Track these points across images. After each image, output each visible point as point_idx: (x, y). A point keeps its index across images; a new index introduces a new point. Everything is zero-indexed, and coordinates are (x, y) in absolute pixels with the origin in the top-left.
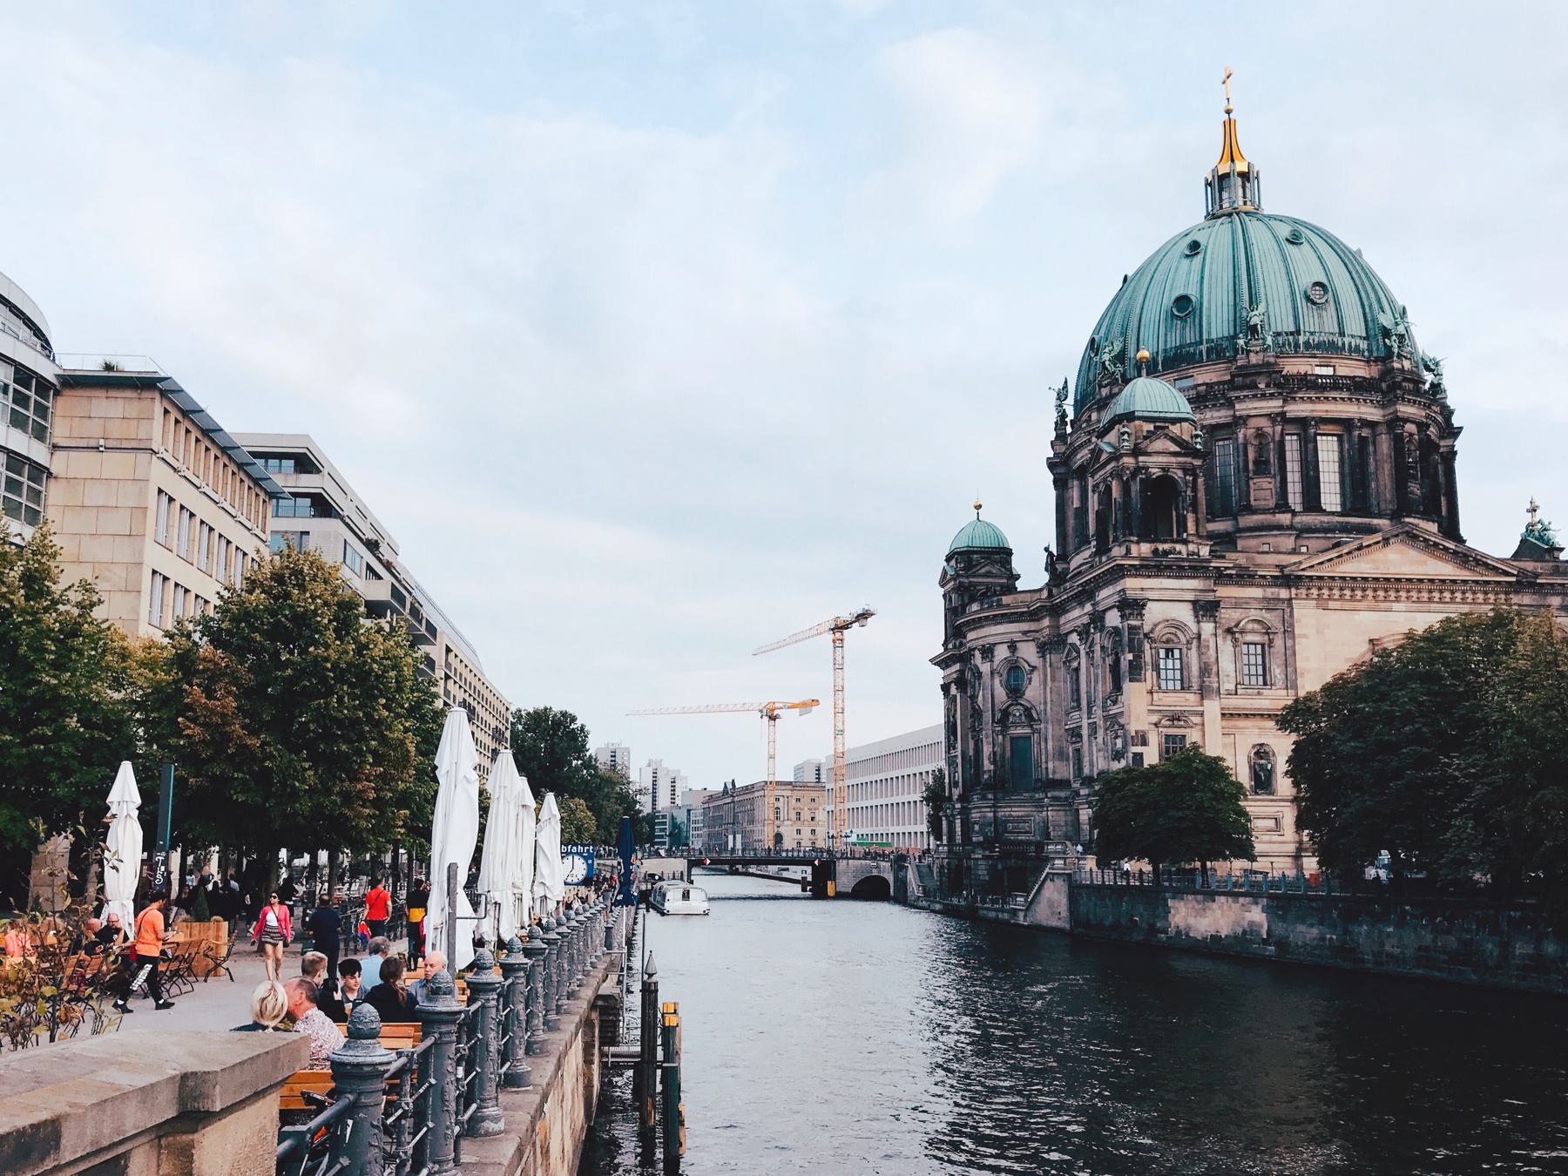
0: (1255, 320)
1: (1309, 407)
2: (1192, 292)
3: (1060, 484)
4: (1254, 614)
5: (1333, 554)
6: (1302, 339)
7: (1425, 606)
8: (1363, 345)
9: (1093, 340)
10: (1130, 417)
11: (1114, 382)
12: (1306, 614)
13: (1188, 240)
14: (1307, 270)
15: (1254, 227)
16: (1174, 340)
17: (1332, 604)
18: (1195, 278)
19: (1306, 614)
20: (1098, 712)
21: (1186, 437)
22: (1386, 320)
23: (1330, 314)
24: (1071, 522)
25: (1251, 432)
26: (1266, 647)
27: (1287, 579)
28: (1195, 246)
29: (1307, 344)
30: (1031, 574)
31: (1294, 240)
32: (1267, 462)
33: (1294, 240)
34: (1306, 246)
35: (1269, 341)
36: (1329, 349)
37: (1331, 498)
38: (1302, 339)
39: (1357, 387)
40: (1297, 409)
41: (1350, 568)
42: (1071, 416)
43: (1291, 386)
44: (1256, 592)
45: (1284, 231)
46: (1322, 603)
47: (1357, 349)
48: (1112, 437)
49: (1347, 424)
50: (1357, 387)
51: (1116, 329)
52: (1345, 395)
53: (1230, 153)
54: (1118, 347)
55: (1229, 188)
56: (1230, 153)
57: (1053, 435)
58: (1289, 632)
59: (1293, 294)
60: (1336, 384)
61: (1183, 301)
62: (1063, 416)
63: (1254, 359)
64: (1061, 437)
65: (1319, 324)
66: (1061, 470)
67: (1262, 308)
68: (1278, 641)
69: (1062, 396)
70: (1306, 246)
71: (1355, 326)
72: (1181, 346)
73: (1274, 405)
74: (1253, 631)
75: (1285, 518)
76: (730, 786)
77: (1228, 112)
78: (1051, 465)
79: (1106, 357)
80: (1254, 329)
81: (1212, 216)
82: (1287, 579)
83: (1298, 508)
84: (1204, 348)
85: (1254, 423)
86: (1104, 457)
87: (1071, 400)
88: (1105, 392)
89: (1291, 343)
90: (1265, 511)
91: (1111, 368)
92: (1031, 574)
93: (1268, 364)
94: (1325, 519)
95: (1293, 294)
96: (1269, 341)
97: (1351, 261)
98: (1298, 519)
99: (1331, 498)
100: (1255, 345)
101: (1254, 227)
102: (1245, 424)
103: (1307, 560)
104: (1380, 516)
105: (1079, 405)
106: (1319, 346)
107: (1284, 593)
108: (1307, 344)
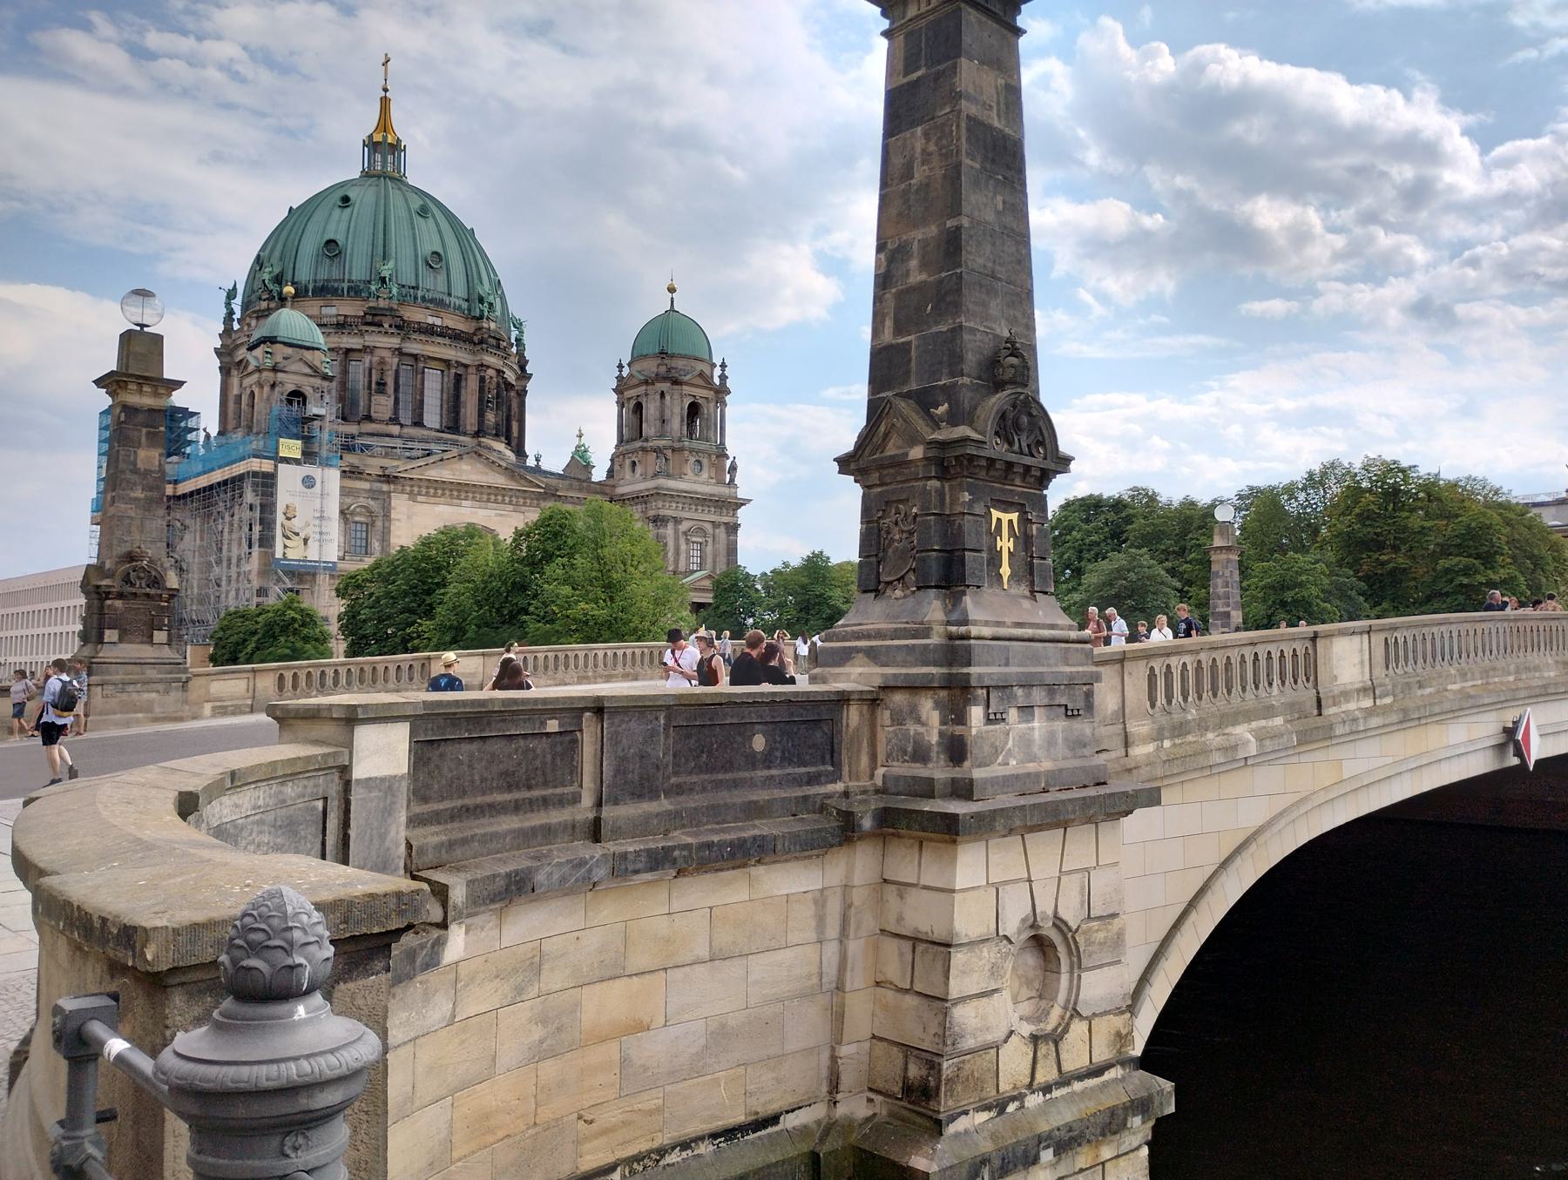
0: (386, 274)
1: (420, 346)
2: (340, 239)
3: (225, 371)
4: (362, 501)
5: (421, 462)
6: (420, 293)
7: (433, 500)
8: (465, 305)
9: (258, 257)
10: (272, 340)
11: (271, 298)
12: (400, 504)
13: (341, 193)
14: (430, 244)
15: (395, 196)
16: (323, 275)
17: (420, 498)
18: (343, 226)
19: (400, 504)
20: (234, 568)
21: (317, 363)
22: (485, 288)
23: (442, 278)
24: (231, 405)
25: (375, 359)
26: (369, 525)
27: (388, 478)
28: (346, 199)
29: (423, 298)
30: (599, 475)
31: (423, 212)
32: (385, 384)
33: (423, 212)
34: (431, 221)
35: (395, 291)
36: (439, 304)
37: (432, 418)
38: (420, 293)
39: (456, 336)
40: (413, 347)
41: (434, 473)
42: (237, 315)
43: (403, 328)
44: (366, 485)
45: (416, 203)
46: (412, 497)
47: (460, 308)
48: (258, 352)
49: (447, 363)
50: (456, 336)
51: (277, 254)
52: (447, 341)
53: (384, 123)
54: (277, 271)
55: (383, 148)
56: (384, 123)
57: (221, 328)
58: (387, 516)
59: (416, 256)
60: (444, 333)
61: (331, 243)
62: (231, 313)
63: (382, 304)
64: (227, 332)
65: (432, 284)
66: (227, 359)
67: (391, 264)
68: (379, 524)
69: (231, 295)
70: (431, 221)
71: (459, 289)
72: (328, 281)
73: (394, 342)
74: (360, 514)
75: (395, 429)
76: (192, 423)
77: (386, 90)
78: (218, 352)
79: (266, 277)
80: (383, 280)
81: (366, 175)
82: (388, 478)
83: (409, 422)
84: (345, 285)
85: (378, 352)
86: (251, 368)
87: (238, 300)
88: (264, 305)
89: (411, 294)
90: (381, 422)
91: (271, 287)
92: (599, 475)
93: (391, 309)
94: (426, 432)
95: (416, 256)
96: (395, 291)
97: (464, 235)
98: (405, 430)
99: (432, 418)
100: (384, 293)
101: (395, 196)
102: (372, 353)
103: (396, 466)
104: (465, 434)
105: (246, 306)
106: (432, 301)
107: (385, 487)
108: (423, 298)
